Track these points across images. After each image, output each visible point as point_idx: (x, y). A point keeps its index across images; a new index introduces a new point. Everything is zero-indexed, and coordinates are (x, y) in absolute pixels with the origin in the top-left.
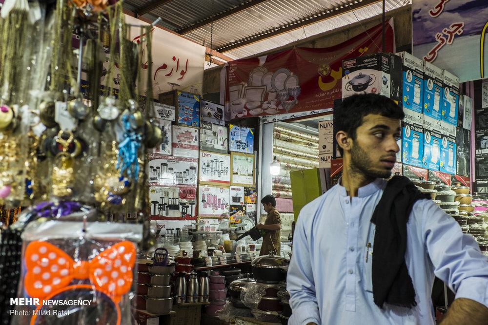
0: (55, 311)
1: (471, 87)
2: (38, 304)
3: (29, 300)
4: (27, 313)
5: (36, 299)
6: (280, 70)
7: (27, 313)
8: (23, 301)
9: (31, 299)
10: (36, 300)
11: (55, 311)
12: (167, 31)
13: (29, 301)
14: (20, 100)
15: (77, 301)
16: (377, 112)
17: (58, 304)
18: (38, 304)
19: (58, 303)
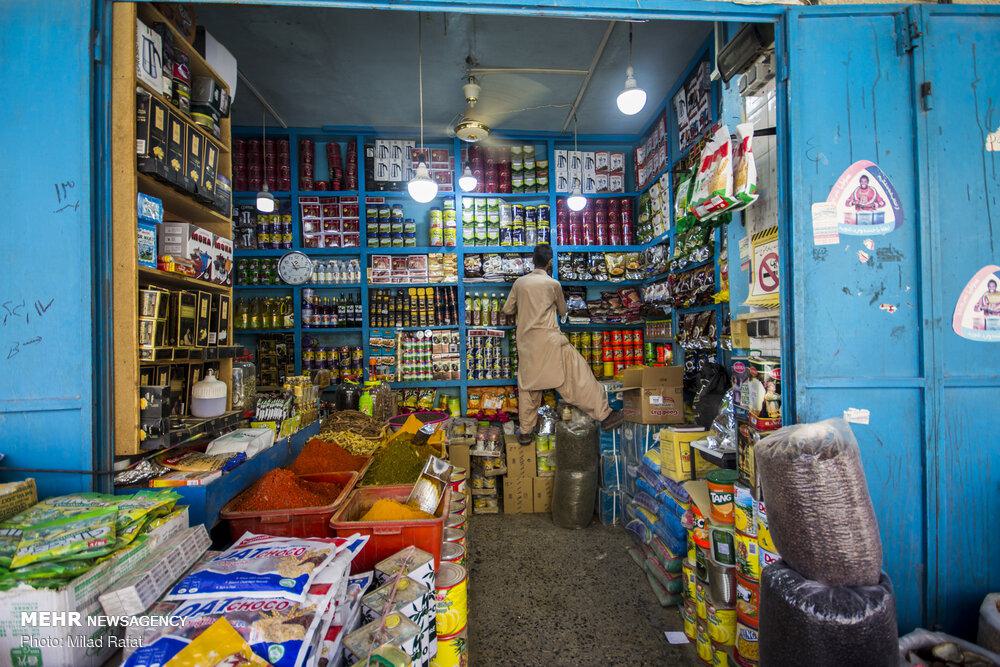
0: (113, 639)
1: (934, 512)
2: (79, 624)
3: (59, 615)
4: (99, 643)
5: (74, 613)
6: (801, 487)
7: (99, 643)
8: (48, 618)
9: (63, 614)
10: (74, 617)
11: (113, 639)
12: (91, 237)
13: (59, 618)
14: (583, 481)
15: (158, 618)
16: (373, 186)
17: (119, 625)
18: (79, 624)
19: (120, 621)
